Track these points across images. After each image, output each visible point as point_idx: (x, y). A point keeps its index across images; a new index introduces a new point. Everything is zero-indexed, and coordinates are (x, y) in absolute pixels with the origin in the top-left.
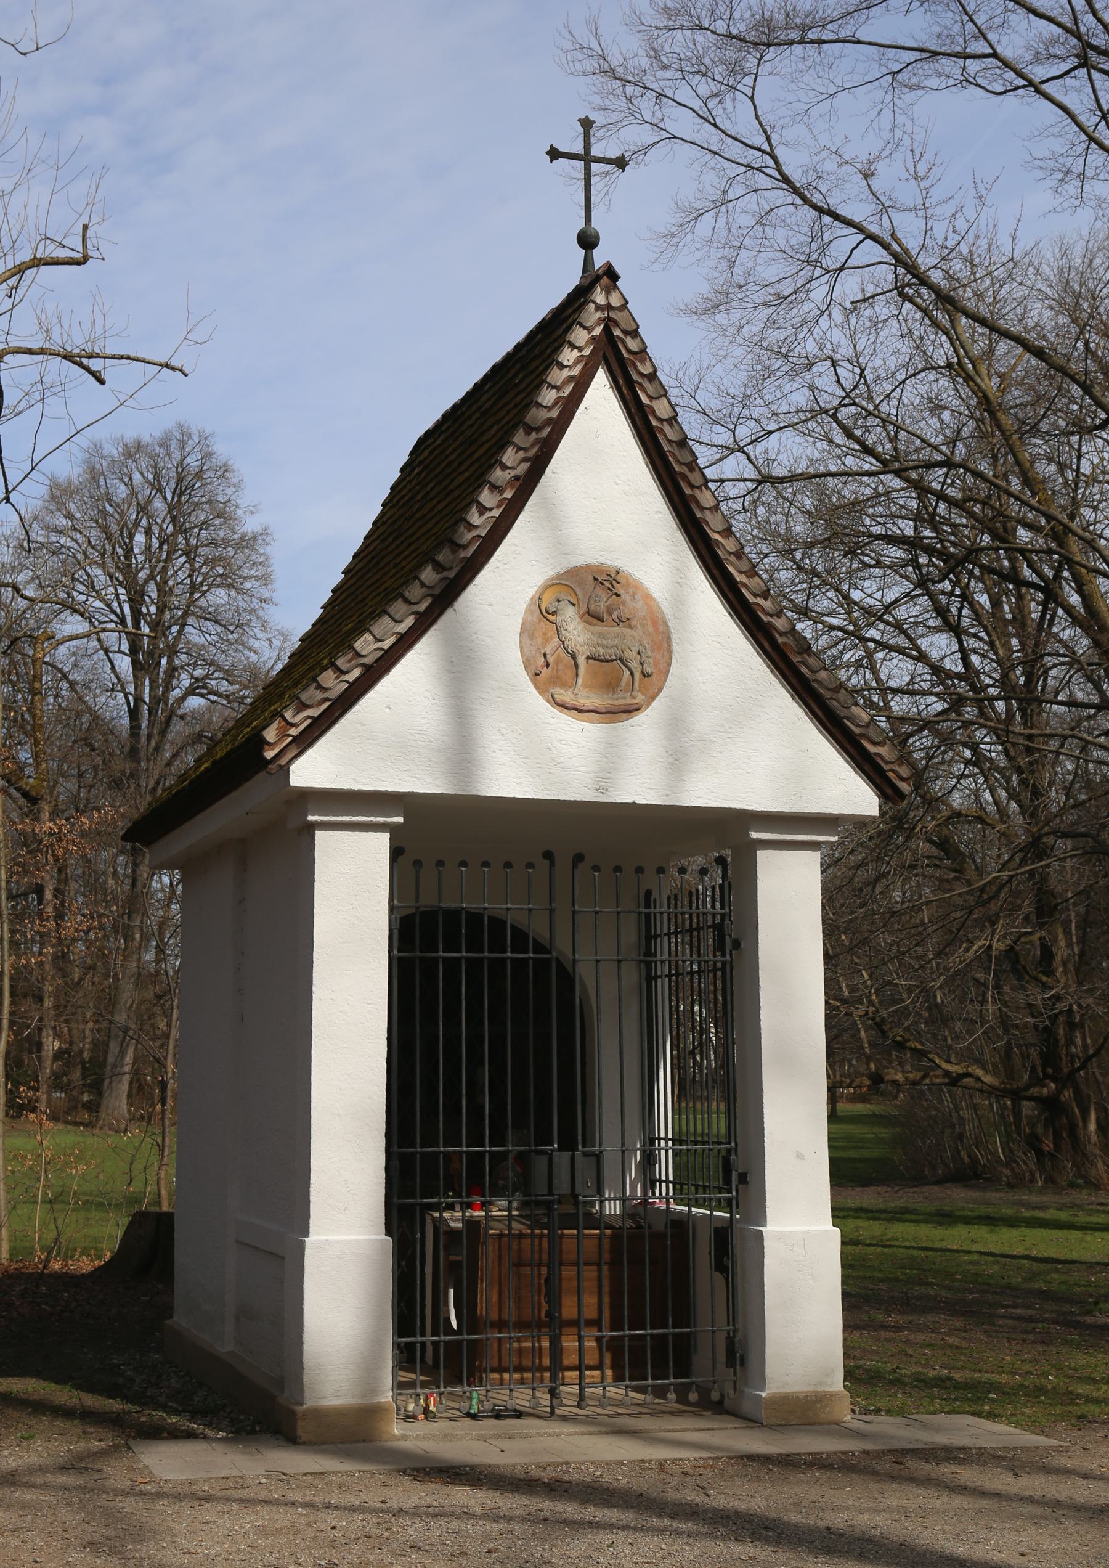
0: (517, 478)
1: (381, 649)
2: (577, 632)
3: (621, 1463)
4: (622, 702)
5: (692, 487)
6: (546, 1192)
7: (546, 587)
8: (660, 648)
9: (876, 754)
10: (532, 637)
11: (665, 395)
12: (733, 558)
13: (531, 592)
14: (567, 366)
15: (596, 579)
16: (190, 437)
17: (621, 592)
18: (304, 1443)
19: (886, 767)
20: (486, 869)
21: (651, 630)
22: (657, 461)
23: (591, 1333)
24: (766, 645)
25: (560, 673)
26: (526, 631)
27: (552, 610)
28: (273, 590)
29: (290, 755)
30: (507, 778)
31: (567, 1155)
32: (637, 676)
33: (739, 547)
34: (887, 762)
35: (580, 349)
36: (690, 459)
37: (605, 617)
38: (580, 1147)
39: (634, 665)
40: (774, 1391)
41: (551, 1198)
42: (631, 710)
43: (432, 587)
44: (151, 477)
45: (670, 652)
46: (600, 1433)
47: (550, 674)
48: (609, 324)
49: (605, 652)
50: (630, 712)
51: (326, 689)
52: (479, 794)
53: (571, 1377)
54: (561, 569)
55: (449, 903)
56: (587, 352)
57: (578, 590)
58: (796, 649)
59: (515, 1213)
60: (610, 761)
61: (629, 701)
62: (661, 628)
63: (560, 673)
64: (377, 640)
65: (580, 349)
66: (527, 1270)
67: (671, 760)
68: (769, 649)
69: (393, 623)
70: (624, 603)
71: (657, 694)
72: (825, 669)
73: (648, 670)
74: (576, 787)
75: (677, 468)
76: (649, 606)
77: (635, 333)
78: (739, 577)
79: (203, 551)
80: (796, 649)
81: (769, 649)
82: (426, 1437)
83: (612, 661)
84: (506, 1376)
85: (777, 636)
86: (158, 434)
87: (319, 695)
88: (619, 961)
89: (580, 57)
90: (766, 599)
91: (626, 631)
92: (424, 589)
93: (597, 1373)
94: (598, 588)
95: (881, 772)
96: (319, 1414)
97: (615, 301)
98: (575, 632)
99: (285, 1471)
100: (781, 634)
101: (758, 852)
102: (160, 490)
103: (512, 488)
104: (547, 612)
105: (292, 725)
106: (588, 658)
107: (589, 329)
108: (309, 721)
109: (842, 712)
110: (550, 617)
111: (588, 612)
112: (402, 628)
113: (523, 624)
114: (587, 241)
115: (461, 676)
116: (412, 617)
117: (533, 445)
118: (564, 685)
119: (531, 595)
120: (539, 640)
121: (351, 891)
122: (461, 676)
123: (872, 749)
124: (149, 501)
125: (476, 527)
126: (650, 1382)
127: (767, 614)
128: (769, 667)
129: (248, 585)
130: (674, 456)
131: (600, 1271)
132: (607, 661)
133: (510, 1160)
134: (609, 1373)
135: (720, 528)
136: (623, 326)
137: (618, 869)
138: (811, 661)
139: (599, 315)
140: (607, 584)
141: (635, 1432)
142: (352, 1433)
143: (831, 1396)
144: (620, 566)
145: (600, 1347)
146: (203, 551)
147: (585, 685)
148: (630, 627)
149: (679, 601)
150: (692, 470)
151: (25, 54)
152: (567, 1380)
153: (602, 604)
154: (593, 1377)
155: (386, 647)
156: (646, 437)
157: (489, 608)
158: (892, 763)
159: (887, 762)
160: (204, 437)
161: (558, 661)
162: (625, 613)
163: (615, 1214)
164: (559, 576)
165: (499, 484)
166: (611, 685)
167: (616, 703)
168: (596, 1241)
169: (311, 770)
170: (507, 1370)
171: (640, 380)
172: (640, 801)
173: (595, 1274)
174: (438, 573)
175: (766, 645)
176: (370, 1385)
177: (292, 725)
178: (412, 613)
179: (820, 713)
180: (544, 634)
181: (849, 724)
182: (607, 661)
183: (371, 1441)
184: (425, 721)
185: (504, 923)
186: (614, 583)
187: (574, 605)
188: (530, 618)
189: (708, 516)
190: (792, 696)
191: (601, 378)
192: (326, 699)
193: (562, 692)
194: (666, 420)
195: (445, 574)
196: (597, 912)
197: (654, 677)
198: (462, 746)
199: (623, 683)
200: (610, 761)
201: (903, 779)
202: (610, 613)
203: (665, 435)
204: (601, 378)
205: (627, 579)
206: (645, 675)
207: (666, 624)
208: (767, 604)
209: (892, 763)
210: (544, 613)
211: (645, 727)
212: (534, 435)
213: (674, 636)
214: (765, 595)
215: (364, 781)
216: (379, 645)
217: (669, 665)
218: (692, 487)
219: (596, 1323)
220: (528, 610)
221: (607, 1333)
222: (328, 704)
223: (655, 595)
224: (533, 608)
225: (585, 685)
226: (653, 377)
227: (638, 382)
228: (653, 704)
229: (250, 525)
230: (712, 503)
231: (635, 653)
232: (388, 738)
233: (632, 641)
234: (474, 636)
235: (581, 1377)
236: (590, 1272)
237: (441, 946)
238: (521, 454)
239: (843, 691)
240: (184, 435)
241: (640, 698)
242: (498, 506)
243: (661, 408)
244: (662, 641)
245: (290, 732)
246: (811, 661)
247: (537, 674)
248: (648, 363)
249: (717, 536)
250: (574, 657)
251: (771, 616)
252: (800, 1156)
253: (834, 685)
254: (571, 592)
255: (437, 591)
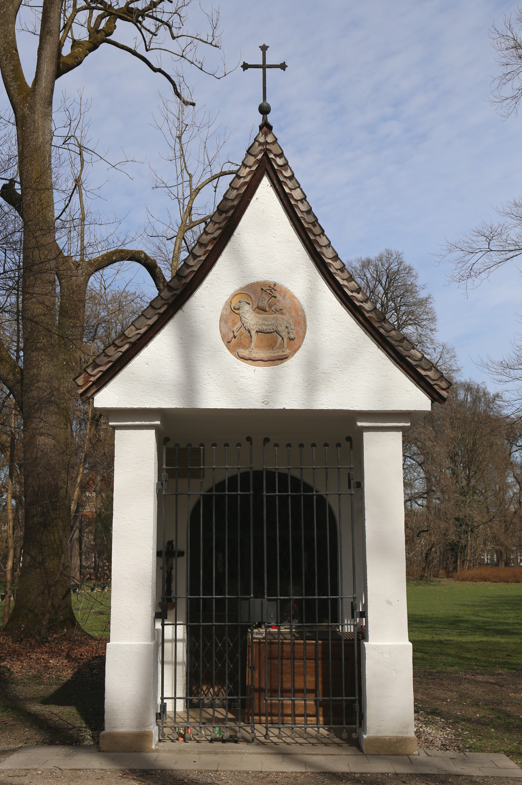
0: (214, 239)
1: (139, 334)
2: (250, 318)
3: (248, 773)
4: (276, 354)
5: (315, 235)
6: (248, 621)
7: (234, 295)
8: (299, 323)
9: (426, 376)
10: (226, 322)
11: (299, 187)
12: (339, 272)
13: (226, 298)
14: (242, 177)
15: (262, 289)
16: (392, 255)
17: (277, 295)
18: (103, 751)
19: (432, 383)
20: (214, 448)
21: (294, 314)
22: (296, 223)
23: (312, 696)
24: (361, 319)
25: (242, 341)
26: (223, 320)
27: (237, 307)
28: (435, 325)
29: (92, 391)
30: (214, 398)
31: (259, 601)
32: (286, 340)
33: (342, 266)
34: (433, 380)
35: (250, 167)
36: (313, 220)
37: (267, 309)
38: (266, 596)
39: (284, 334)
40: (372, 735)
41: (249, 624)
42: (283, 359)
43: (168, 299)
44: (375, 276)
45: (305, 326)
46: (268, 753)
47: (236, 342)
48: (266, 152)
49: (269, 326)
50: (282, 359)
51: (110, 356)
52: (196, 407)
53: (299, 720)
54: (242, 285)
55: (257, 467)
56: (254, 168)
57: (252, 296)
58: (376, 319)
59: (294, 630)
60: (273, 386)
61: (281, 353)
62: (300, 313)
63: (242, 341)
64: (137, 329)
65: (250, 167)
66: (276, 662)
67: (306, 384)
68: (363, 321)
69: (146, 320)
70: (278, 301)
71: (298, 349)
72: (394, 329)
73: (292, 336)
74: (253, 401)
75: (306, 226)
76: (293, 301)
77: (281, 155)
78: (341, 282)
79: (403, 308)
80: (376, 319)
81: (363, 321)
82: (169, 751)
83: (271, 332)
84: (263, 718)
85: (365, 313)
86: (377, 255)
87: (106, 360)
88: (177, 495)
89: (503, 40)
90: (358, 293)
91: (279, 316)
92: (163, 301)
93: (314, 719)
94: (263, 294)
95: (431, 386)
96: (114, 737)
97: (270, 139)
98: (249, 318)
99: (60, 768)
100: (368, 312)
101: (364, 433)
102: (380, 281)
103: (212, 244)
104: (234, 309)
105: (92, 376)
106: (257, 332)
107: (255, 156)
108: (101, 373)
109: (405, 353)
110: (237, 311)
111: (258, 307)
112: (151, 322)
113: (221, 316)
114: (264, 110)
115: (189, 345)
116: (157, 316)
117: (223, 221)
118: (245, 347)
119: (225, 300)
120: (230, 324)
121: (136, 459)
122: (189, 345)
123: (423, 373)
124: (375, 287)
125: (192, 266)
126: (345, 726)
127: (359, 301)
128: (364, 331)
129: (424, 323)
130: (304, 219)
131: (316, 663)
132: (268, 333)
133: (291, 603)
134: (321, 719)
135: (331, 256)
136: (274, 152)
137: (289, 445)
138: (386, 325)
139: (261, 148)
140: (268, 291)
141: (288, 754)
142: (127, 750)
143: (406, 739)
144: (276, 281)
145: (316, 704)
146: (403, 308)
147: (256, 347)
148: (282, 314)
149: (312, 298)
150: (314, 226)
151: (219, 78)
152: (297, 722)
153: (266, 302)
154: (311, 720)
155: (142, 333)
156: (290, 211)
157: (202, 309)
158: (436, 380)
159: (433, 380)
160: (398, 255)
161: (241, 335)
162: (279, 306)
163: (351, 633)
164: (242, 289)
165: (204, 242)
166: (271, 346)
167: (273, 355)
168: (314, 647)
169: (106, 398)
170: (264, 715)
171: (284, 180)
172: (288, 407)
173: (314, 665)
174: (170, 292)
175: (361, 319)
176: (143, 721)
177: (92, 376)
178: (156, 314)
179: (393, 355)
180: (233, 321)
181: (409, 359)
182: (268, 333)
183: (140, 752)
184: (167, 370)
185: (287, 475)
186: (273, 290)
187: (249, 304)
188: (225, 313)
189: (324, 250)
190: (378, 346)
191: (265, 181)
192: (110, 361)
193: (243, 351)
194: (300, 200)
195: (174, 292)
196: (314, 469)
197: (296, 340)
198: (190, 381)
199: (278, 344)
200: (273, 386)
201: (443, 389)
202: (270, 307)
203: (299, 209)
204: (265, 181)
205: (280, 288)
206: (291, 339)
207: (304, 311)
208: (359, 296)
209: (436, 380)
210: (233, 310)
211: (293, 366)
212: (224, 215)
213: (307, 317)
214: (359, 290)
215: (134, 403)
216: (138, 331)
217: (305, 333)
218: (315, 235)
219: (314, 691)
220: (224, 308)
221: (320, 698)
222: (111, 364)
223: (296, 296)
224: (227, 307)
225: (256, 347)
226: (292, 178)
227: (283, 182)
228: (296, 355)
229: (422, 294)
230: (327, 243)
231: (284, 328)
232: (149, 379)
233: (281, 322)
234: (194, 324)
235: (306, 721)
236: (311, 664)
237: (302, 489)
238: (217, 226)
239: (405, 341)
240: (389, 253)
241: (287, 352)
242: (204, 254)
243: (297, 194)
244: (301, 322)
245: (91, 379)
246: (386, 325)
247: (229, 342)
248: (289, 170)
249: (330, 261)
250: (249, 332)
251: (362, 302)
252: (389, 603)
253: (400, 339)
254: (248, 297)
255: (170, 301)
